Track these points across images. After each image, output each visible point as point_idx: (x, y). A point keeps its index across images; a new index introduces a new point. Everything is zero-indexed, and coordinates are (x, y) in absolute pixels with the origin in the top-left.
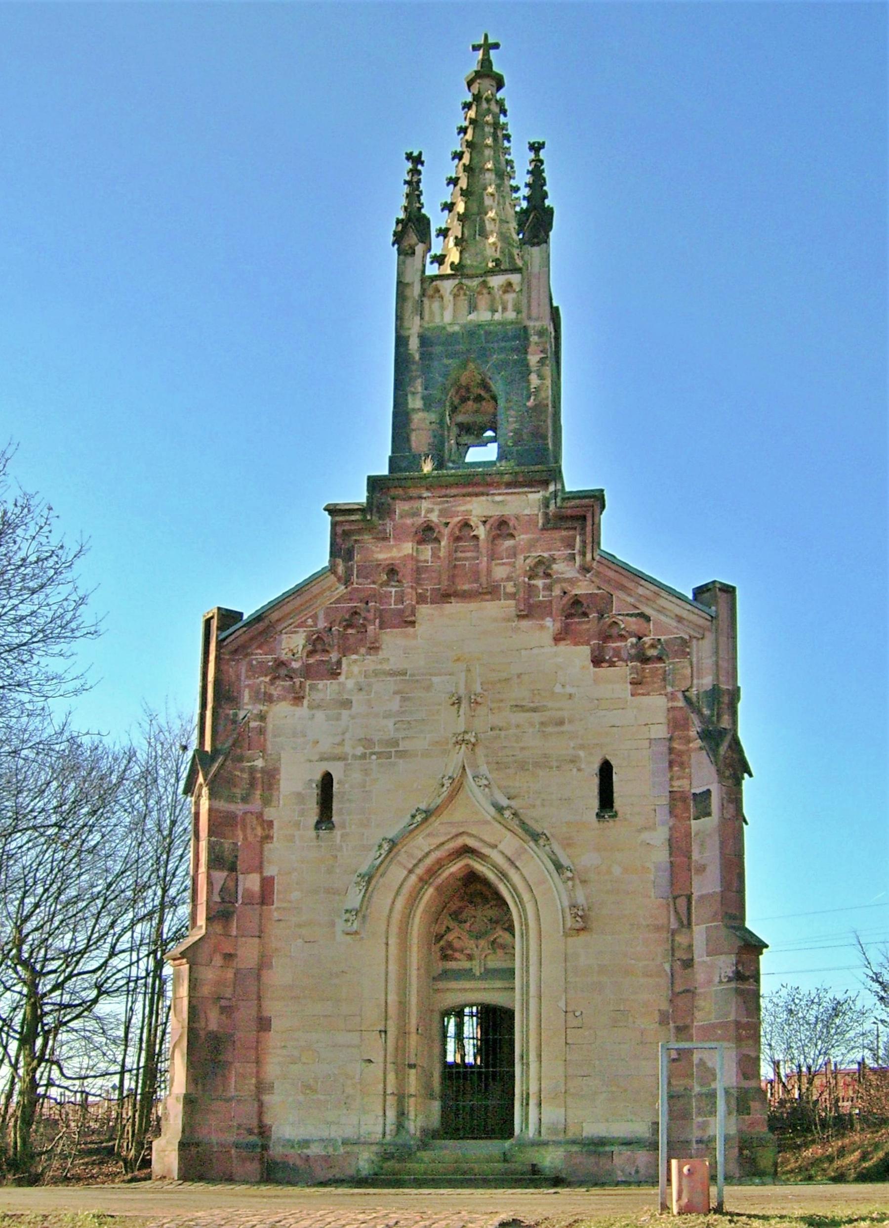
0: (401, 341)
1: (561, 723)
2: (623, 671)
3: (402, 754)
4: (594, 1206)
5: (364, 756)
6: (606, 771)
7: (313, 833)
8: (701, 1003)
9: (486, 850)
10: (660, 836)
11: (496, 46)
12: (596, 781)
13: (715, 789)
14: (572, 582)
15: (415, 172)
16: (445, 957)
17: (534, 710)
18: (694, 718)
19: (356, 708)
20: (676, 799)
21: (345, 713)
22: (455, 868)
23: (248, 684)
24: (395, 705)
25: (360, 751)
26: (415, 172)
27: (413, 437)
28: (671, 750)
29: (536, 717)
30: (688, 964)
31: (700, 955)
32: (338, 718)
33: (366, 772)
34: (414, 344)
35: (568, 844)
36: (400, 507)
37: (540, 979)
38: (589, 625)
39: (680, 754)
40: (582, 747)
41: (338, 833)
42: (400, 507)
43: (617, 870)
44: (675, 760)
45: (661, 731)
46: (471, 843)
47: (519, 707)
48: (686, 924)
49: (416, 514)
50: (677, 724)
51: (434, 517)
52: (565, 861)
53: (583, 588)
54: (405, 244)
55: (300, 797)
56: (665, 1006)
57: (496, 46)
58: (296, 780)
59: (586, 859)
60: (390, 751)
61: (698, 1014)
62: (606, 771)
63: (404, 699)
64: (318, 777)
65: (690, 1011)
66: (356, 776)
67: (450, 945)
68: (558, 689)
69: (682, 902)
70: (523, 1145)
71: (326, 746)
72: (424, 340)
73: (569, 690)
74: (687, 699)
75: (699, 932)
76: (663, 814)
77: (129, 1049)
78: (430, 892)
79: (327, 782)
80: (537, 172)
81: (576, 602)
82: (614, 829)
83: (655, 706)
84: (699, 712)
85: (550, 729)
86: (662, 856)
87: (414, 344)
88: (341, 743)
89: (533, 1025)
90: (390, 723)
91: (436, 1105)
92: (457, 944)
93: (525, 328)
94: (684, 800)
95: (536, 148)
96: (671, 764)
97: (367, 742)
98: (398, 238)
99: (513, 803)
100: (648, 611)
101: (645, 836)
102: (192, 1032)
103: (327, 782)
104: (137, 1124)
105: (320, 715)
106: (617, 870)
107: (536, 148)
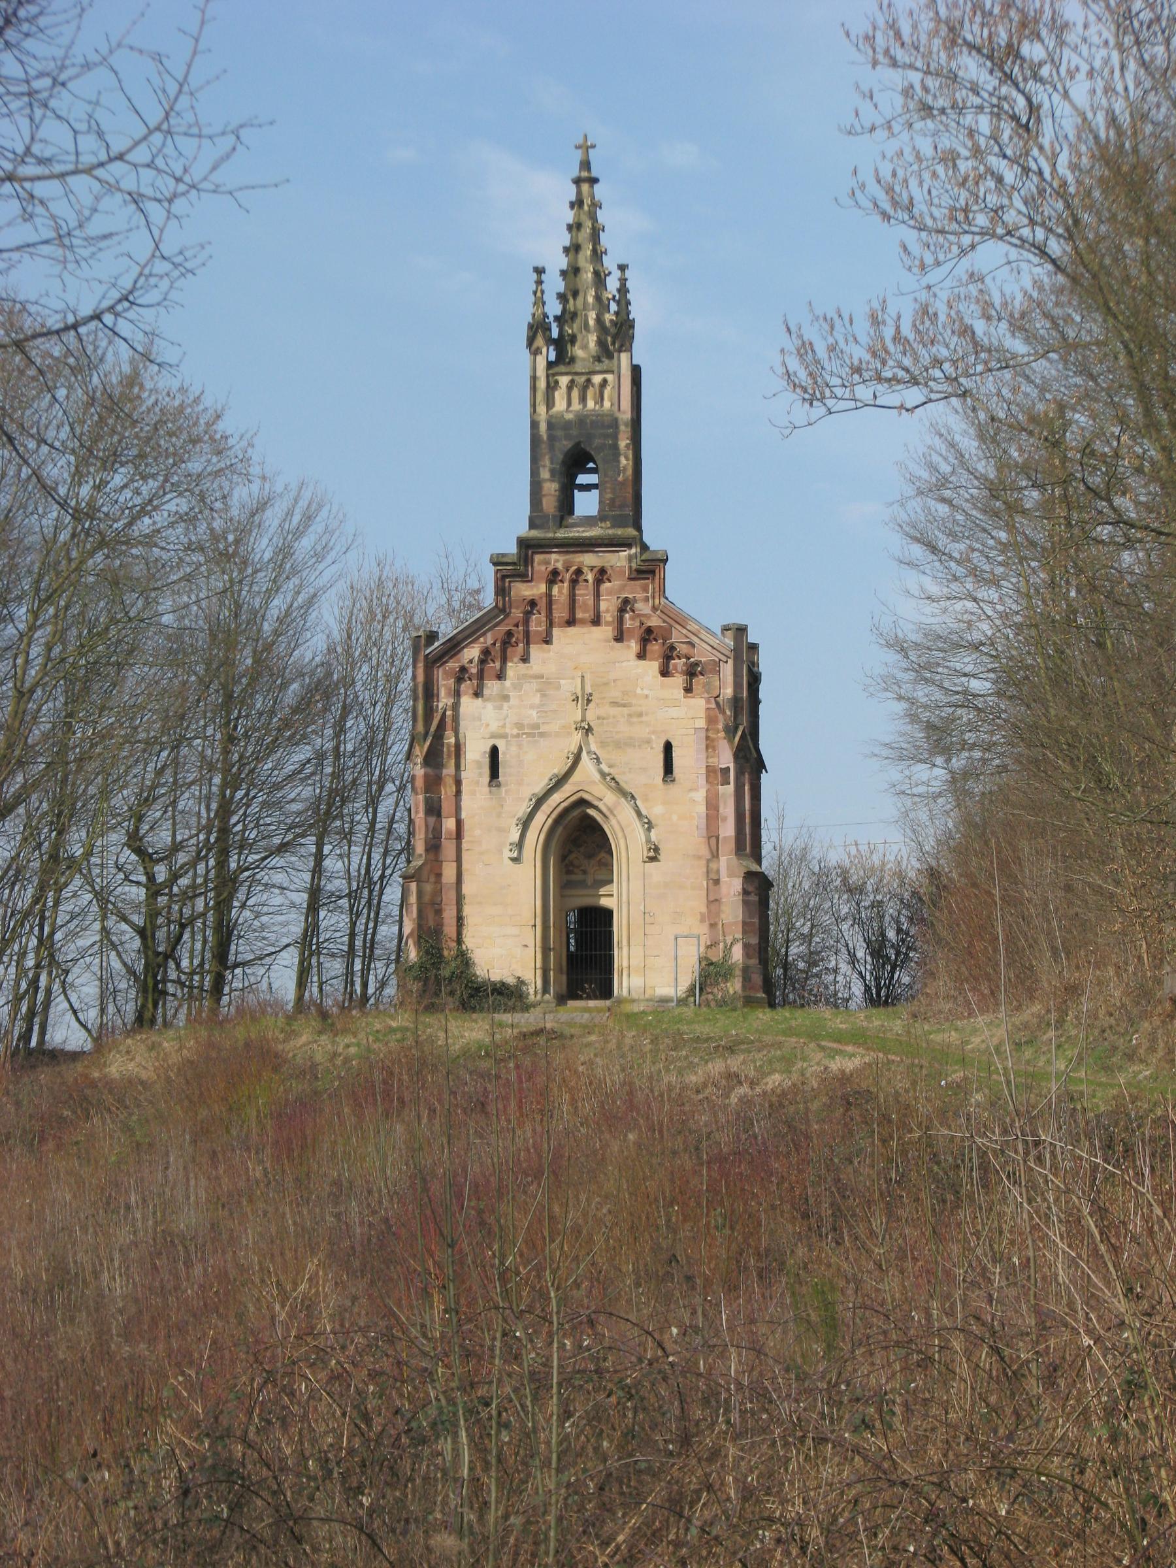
0: (534, 425)
1: (640, 715)
2: (678, 680)
3: (542, 735)
4: (334, 510)
5: (518, 736)
6: (668, 748)
7: (487, 789)
8: (723, 908)
9: (596, 803)
10: (700, 795)
11: (593, 146)
12: (661, 756)
13: (732, 766)
14: (648, 616)
15: (539, 282)
16: (569, 872)
17: (624, 706)
18: (721, 717)
19: (513, 701)
20: (710, 770)
21: (506, 705)
22: (576, 813)
23: (444, 684)
24: (537, 700)
25: (515, 731)
26: (539, 282)
27: (544, 501)
28: (707, 738)
29: (626, 710)
30: (717, 882)
31: (724, 878)
32: (501, 708)
33: (520, 746)
34: (543, 427)
35: (646, 800)
36: (538, 558)
37: (628, 894)
38: (655, 648)
39: (713, 740)
40: (654, 732)
41: (503, 789)
42: (538, 558)
43: (675, 818)
44: (710, 744)
45: (702, 723)
46: (586, 797)
47: (615, 704)
48: (715, 855)
49: (548, 563)
50: (711, 720)
51: (560, 566)
52: (644, 812)
53: (654, 622)
54: (535, 346)
55: (478, 764)
56: (704, 910)
57: (593, 146)
58: (475, 753)
59: (655, 811)
60: (534, 732)
61: (723, 916)
62: (668, 748)
63: (543, 696)
64: (488, 750)
65: (718, 914)
66: (514, 749)
67: (571, 864)
68: (639, 691)
69: (713, 841)
70: (620, 1001)
71: (494, 727)
72: (550, 425)
73: (646, 692)
74: (717, 704)
75: (723, 860)
76: (702, 780)
77: (297, 929)
78: (560, 829)
79: (494, 751)
80: (623, 281)
81: (649, 630)
82: (674, 790)
83: (698, 705)
84: (724, 713)
85: (635, 719)
86: (702, 809)
87: (543, 427)
88: (504, 726)
89: (624, 922)
90: (534, 713)
91: (564, 977)
92: (576, 863)
93: (616, 420)
94: (715, 772)
95: (622, 268)
96: (707, 747)
97: (519, 725)
98: (531, 341)
99: (612, 771)
100: (695, 639)
101: (693, 795)
102: (420, 926)
103: (494, 751)
104: (36, 1028)
105: (490, 706)
106: (675, 818)
107: (622, 268)
